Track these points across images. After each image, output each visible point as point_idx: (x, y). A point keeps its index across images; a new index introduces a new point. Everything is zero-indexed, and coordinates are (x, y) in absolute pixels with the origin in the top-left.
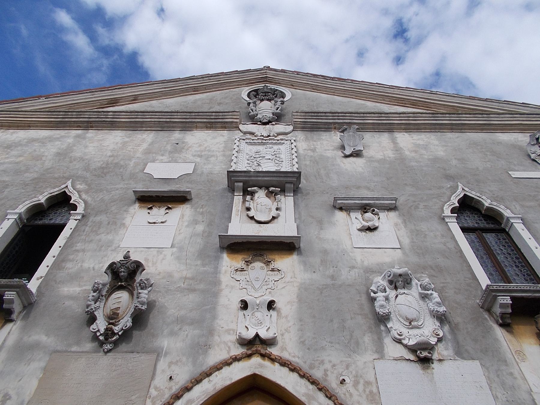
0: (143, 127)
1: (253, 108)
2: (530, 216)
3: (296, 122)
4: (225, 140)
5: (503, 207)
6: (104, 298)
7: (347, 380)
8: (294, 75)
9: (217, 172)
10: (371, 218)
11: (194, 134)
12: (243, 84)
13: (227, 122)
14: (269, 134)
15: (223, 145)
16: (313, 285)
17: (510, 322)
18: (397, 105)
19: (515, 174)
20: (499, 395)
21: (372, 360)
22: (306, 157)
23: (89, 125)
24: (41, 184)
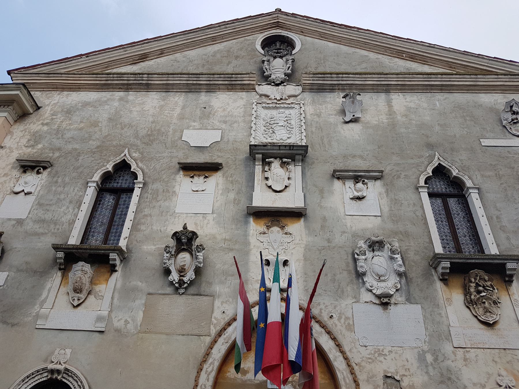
0: (173, 89)
1: (267, 66)
2: (485, 187)
3: (305, 83)
4: (244, 103)
5: (466, 177)
6: (173, 257)
7: (334, 316)
8: (303, 20)
9: (241, 140)
10: (361, 188)
11: (218, 97)
12: (257, 31)
13: (245, 84)
14: (281, 98)
15: (242, 109)
16: (315, 246)
17: (448, 278)
18: (398, 58)
19: (485, 142)
20: (429, 327)
21: (351, 303)
22: (313, 123)
23: (129, 87)
24: (105, 152)
